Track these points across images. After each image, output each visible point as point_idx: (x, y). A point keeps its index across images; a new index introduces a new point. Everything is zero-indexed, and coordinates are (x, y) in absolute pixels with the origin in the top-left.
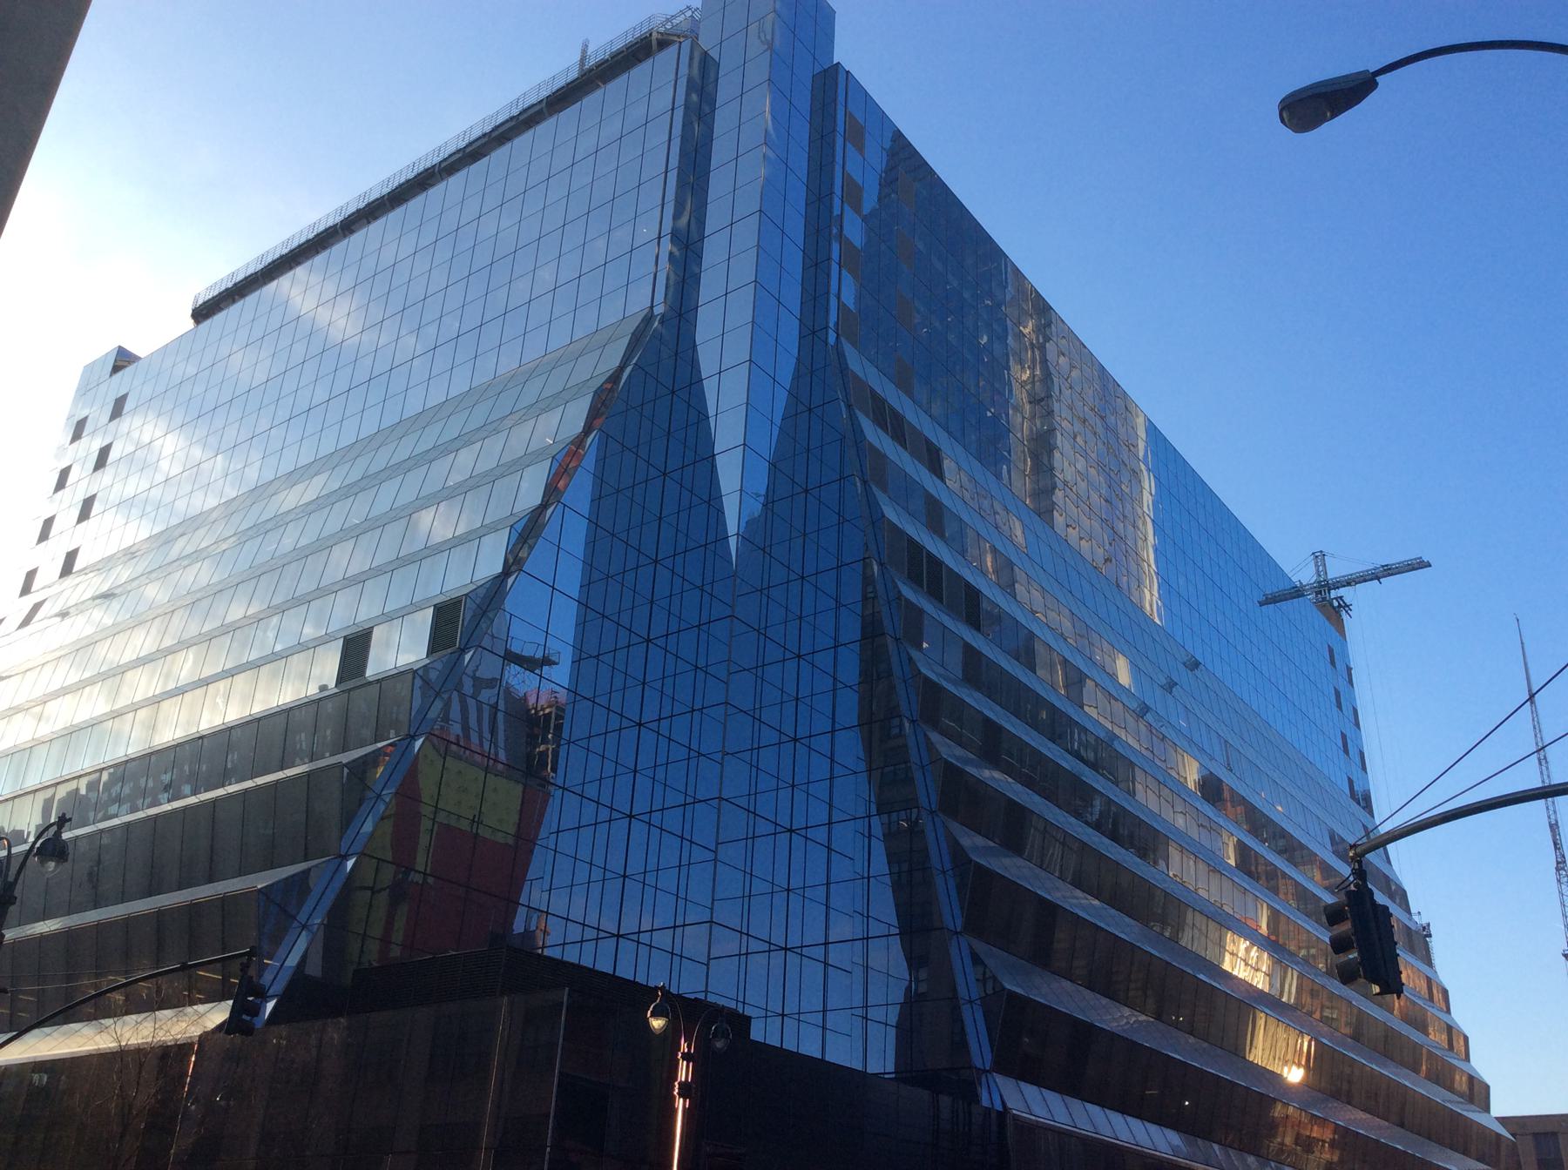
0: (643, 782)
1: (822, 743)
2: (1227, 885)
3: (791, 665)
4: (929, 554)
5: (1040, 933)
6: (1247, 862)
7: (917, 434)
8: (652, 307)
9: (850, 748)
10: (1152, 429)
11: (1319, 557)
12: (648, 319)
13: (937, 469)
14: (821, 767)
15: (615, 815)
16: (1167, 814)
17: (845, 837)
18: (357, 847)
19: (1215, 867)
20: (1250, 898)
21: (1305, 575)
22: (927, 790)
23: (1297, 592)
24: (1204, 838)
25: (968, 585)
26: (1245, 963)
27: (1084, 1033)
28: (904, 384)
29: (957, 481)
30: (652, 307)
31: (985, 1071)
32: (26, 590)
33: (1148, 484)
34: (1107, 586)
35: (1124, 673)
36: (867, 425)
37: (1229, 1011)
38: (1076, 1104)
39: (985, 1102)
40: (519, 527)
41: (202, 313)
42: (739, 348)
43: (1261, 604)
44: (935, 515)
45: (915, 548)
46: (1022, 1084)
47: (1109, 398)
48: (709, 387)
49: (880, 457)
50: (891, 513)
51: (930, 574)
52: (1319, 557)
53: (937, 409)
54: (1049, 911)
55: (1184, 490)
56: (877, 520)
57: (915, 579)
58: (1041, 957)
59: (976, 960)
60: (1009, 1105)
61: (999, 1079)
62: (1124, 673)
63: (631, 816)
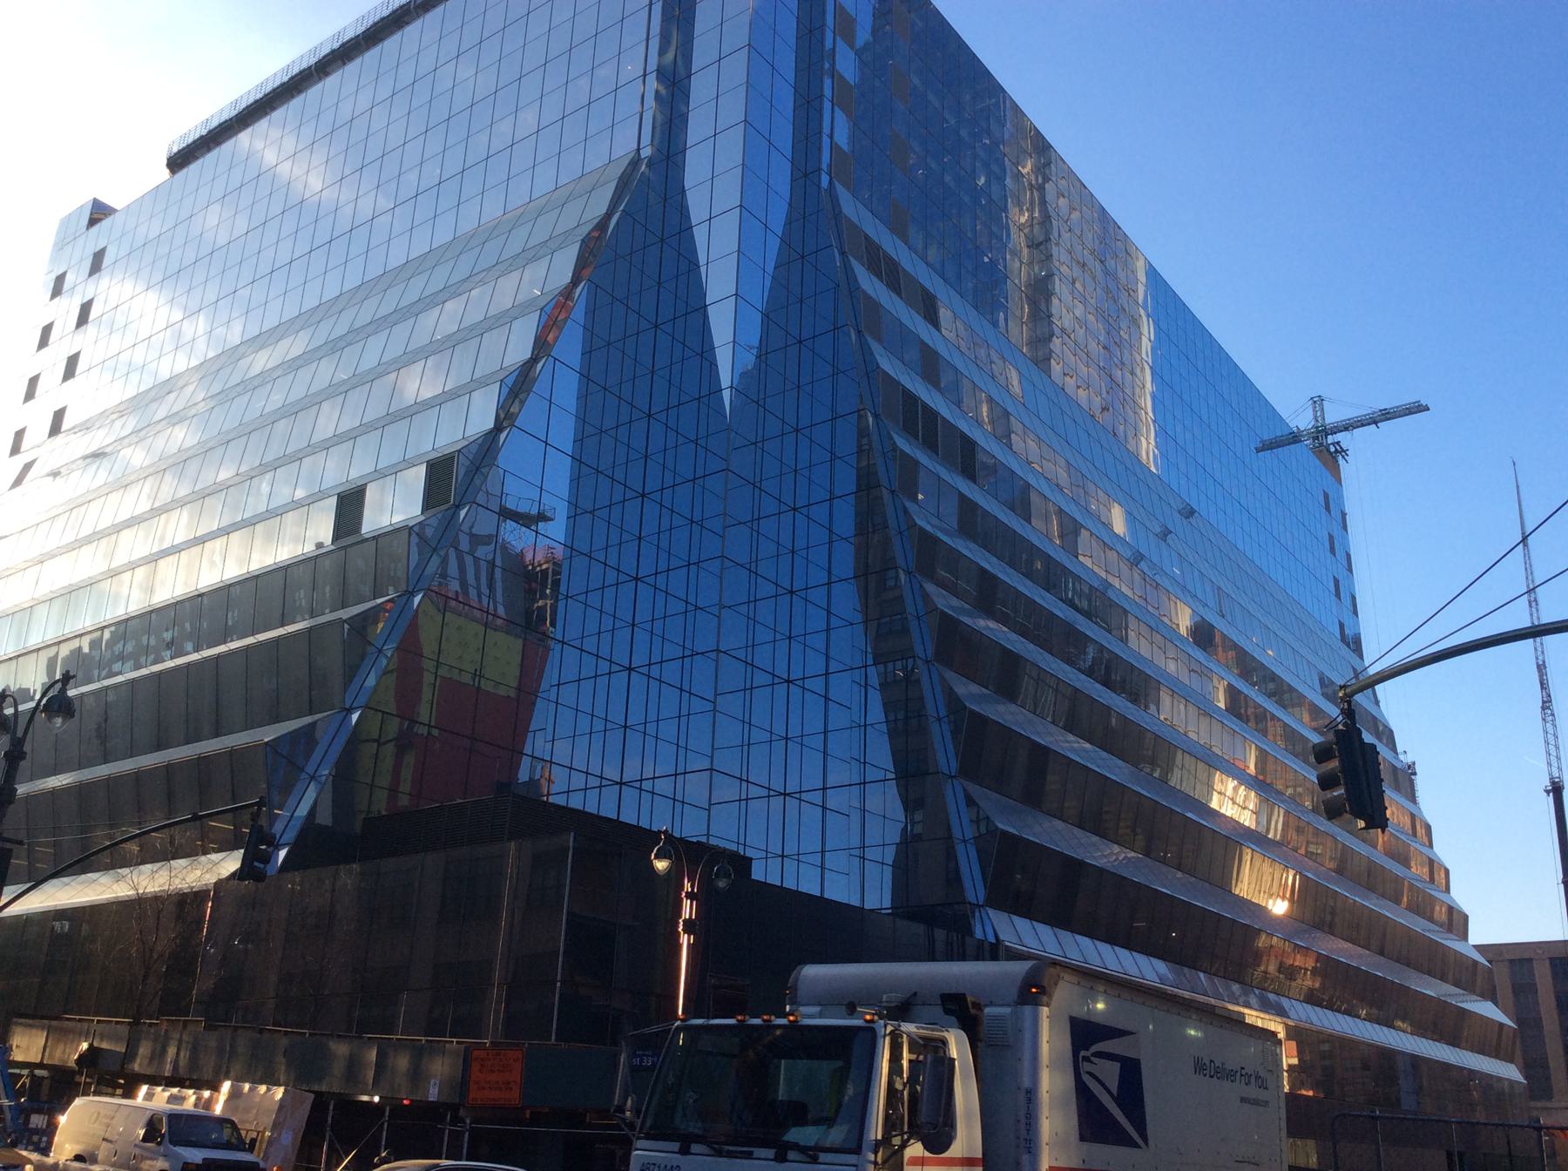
0: (641, 636)
1: (818, 596)
2: (1217, 727)
3: (787, 518)
4: (925, 406)
5: (1033, 776)
6: (1237, 705)
7: (912, 281)
8: (638, 150)
9: (847, 600)
10: (1152, 273)
11: (1318, 402)
12: (635, 162)
13: (933, 320)
14: (817, 620)
15: (615, 668)
16: (1160, 660)
17: (844, 687)
18: (362, 700)
19: (1206, 710)
20: (1239, 740)
21: (1303, 421)
22: (922, 642)
23: (1294, 438)
24: (1194, 682)
25: (963, 436)
26: (1232, 802)
27: (1074, 868)
28: (899, 230)
29: (954, 330)
30: (638, 150)
31: (978, 906)
32: (15, 450)
33: (1147, 330)
34: (1103, 436)
35: (1119, 525)
36: (869, 283)
37: (1218, 847)
38: (1065, 935)
39: (979, 934)
40: (510, 382)
41: (179, 161)
42: (729, 193)
43: (1258, 450)
44: (930, 365)
45: (910, 399)
46: (1015, 918)
47: (1110, 240)
48: (700, 235)
49: (874, 306)
50: (887, 364)
51: (925, 426)
52: (1318, 402)
53: (933, 254)
54: (1041, 754)
55: (1185, 336)
56: (871, 370)
57: (910, 430)
58: (1033, 797)
59: (970, 802)
60: (1002, 937)
61: (991, 912)
62: (1119, 525)
63: (630, 669)
